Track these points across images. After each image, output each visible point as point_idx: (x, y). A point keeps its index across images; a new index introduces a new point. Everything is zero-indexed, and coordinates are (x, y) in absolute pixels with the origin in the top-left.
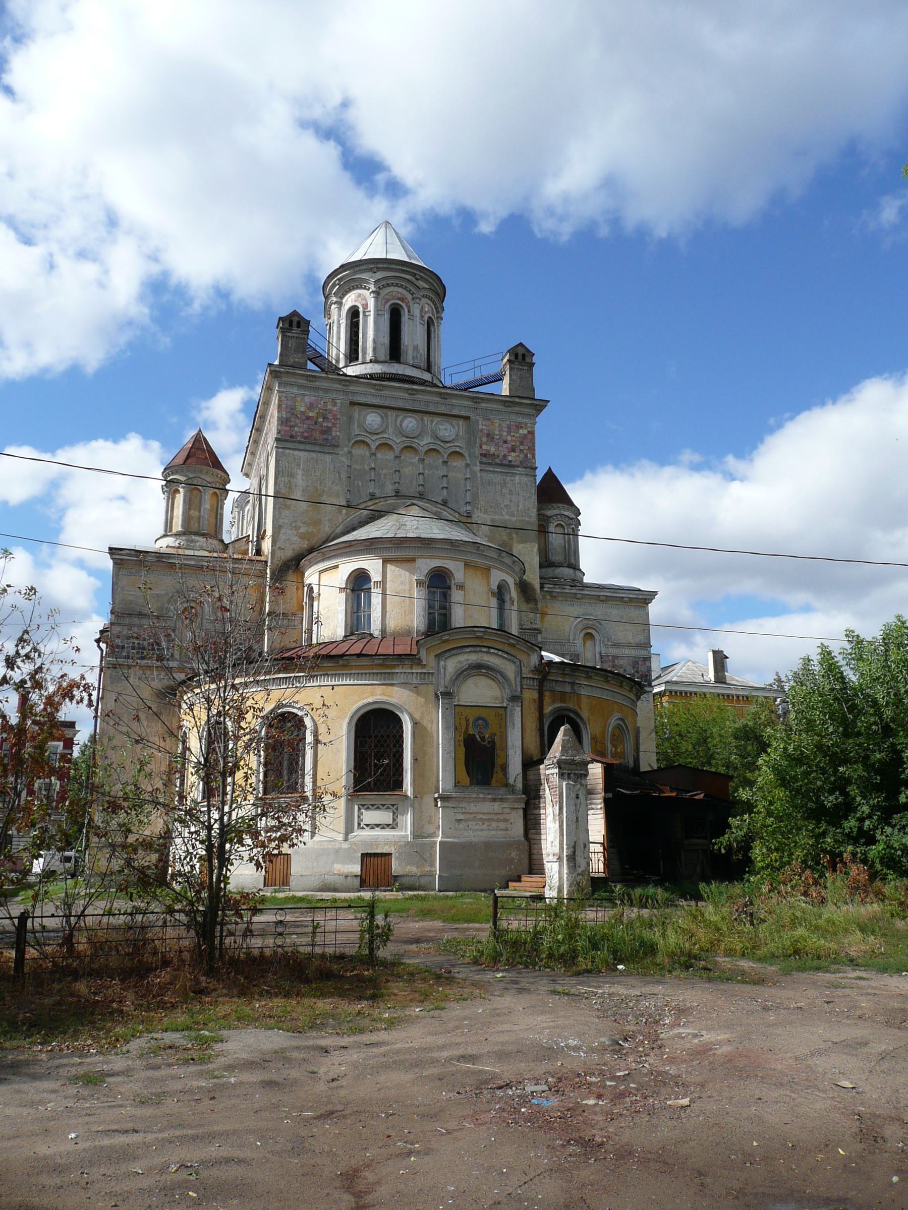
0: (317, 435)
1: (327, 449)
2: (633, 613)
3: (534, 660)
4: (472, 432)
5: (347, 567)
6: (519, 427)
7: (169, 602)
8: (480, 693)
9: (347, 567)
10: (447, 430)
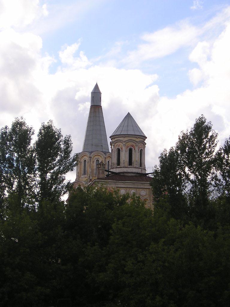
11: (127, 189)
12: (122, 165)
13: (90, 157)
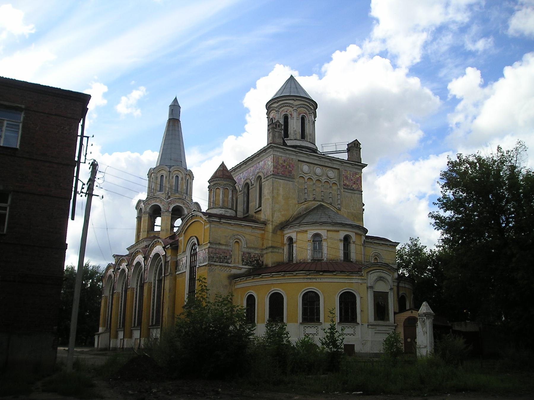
0: (287, 173)
1: (290, 180)
2: (390, 249)
3: (396, 275)
4: (340, 175)
5: (312, 231)
6: (356, 174)
7: (230, 239)
8: (381, 287)
9: (312, 231)
10: (331, 174)
11: (311, 165)
12: (291, 136)
13: (169, 171)
